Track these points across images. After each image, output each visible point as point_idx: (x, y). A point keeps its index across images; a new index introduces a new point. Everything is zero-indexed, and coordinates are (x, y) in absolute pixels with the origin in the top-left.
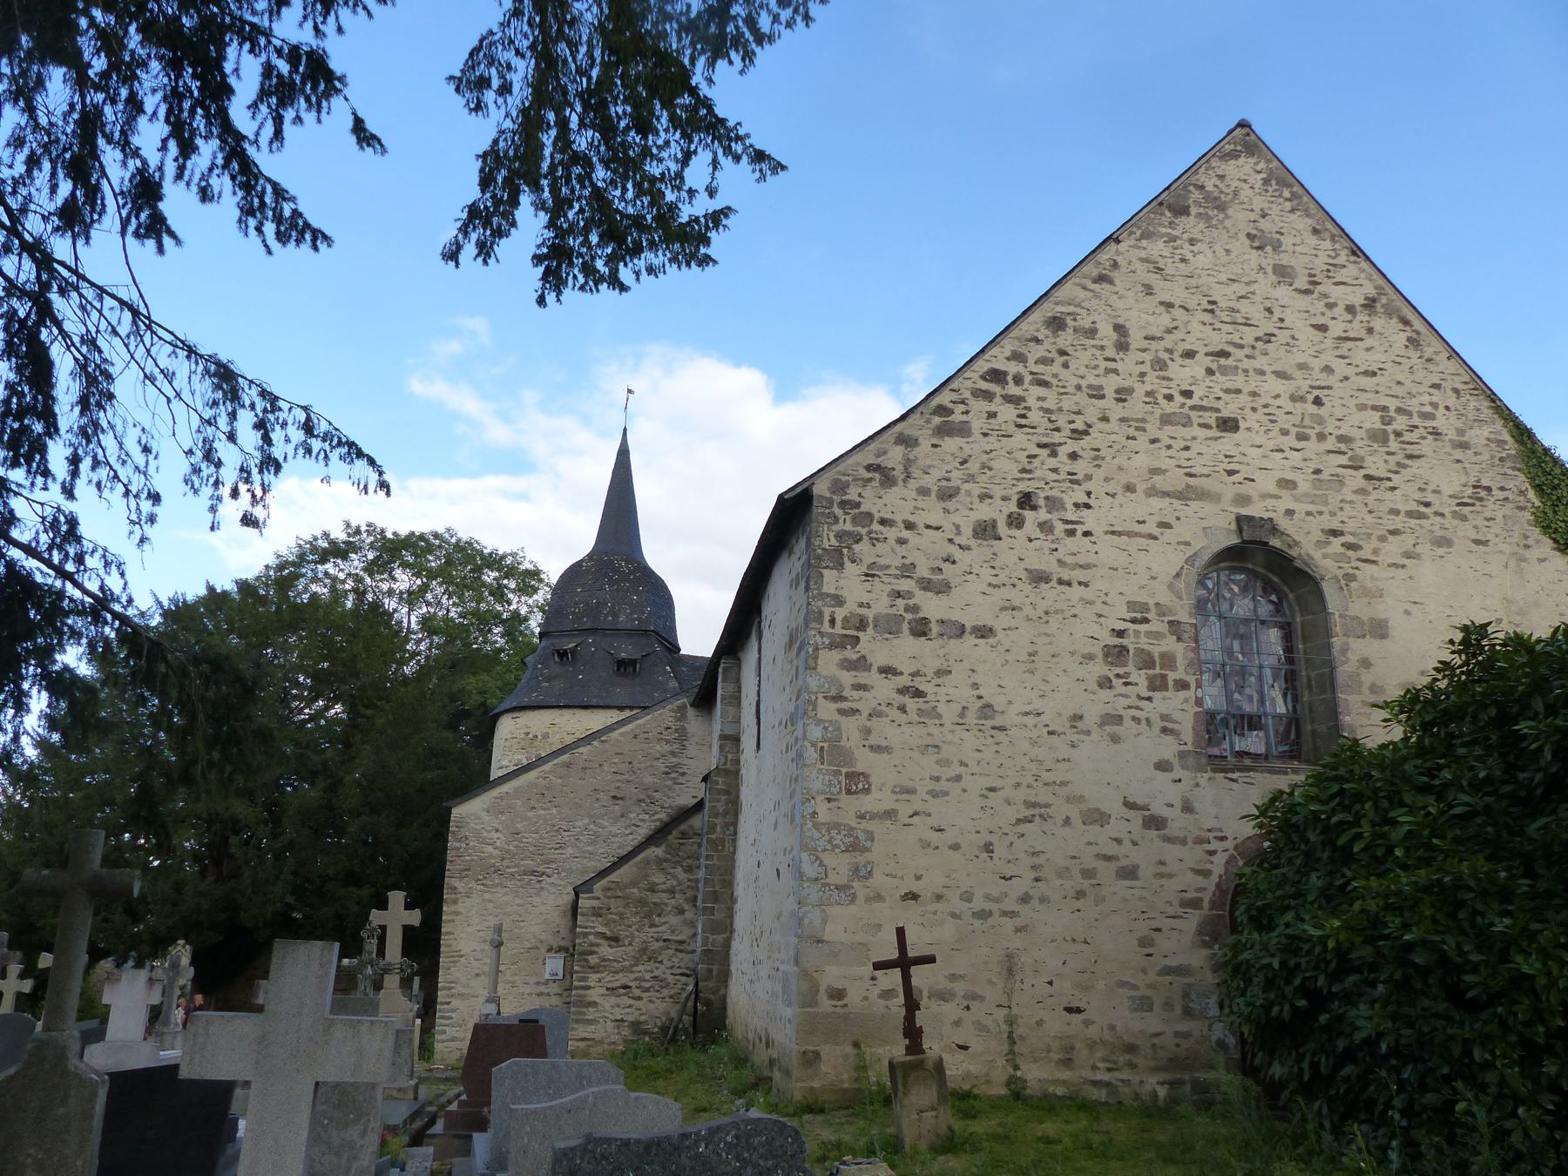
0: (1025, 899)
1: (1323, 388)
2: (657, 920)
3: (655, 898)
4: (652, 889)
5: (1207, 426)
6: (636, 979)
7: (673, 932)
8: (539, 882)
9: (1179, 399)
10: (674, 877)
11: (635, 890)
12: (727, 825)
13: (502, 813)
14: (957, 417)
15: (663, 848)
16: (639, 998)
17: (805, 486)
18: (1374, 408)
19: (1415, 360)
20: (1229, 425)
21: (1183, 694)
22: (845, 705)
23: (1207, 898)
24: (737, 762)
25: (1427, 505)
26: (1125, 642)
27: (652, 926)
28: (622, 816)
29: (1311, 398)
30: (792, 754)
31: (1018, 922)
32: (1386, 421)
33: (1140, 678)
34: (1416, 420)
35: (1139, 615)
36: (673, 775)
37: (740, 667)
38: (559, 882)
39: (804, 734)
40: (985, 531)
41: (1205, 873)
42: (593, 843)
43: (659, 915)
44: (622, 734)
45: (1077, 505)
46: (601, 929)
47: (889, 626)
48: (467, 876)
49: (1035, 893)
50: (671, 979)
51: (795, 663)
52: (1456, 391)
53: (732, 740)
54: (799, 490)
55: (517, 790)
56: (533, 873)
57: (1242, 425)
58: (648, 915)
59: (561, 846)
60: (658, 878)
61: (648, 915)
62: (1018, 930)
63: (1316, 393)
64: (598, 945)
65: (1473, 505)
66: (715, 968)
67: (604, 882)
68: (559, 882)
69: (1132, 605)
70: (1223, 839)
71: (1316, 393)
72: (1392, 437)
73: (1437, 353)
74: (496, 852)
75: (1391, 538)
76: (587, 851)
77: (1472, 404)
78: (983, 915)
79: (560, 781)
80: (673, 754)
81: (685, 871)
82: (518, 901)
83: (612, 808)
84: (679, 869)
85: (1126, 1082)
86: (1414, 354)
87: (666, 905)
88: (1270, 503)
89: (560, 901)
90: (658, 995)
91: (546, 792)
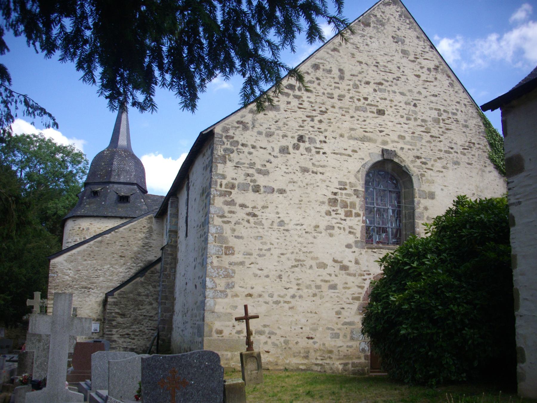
0: (293, 297)
2: (141, 307)
4: (139, 294)
6: (132, 331)
7: (148, 312)
8: (89, 291)
9: (363, 101)
10: (148, 290)
11: (132, 295)
12: (171, 268)
13: (72, 262)
15: (144, 278)
16: (134, 339)
17: (211, 129)
18: (436, 109)
19: (451, 92)
20: (381, 112)
21: (357, 219)
22: (225, 219)
24: (176, 242)
25: (452, 148)
26: (337, 197)
27: (139, 310)
28: (124, 264)
29: (412, 104)
31: (290, 305)
32: (440, 115)
34: (450, 115)
35: (343, 187)
36: (146, 247)
37: (178, 202)
40: (284, 150)
42: (111, 275)
43: (142, 305)
44: (125, 229)
45: (321, 141)
46: (117, 311)
47: (244, 188)
48: (57, 289)
50: (147, 331)
51: (205, 202)
52: (465, 105)
53: (174, 233)
54: (209, 130)
55: (79, 252)
56: (86, 288)
57: (386, 113)
58: (137, 305)
59: (98, 277)
60: (141, 290)
61: (137, 305)
63: (415, 102)
64: (116, 317)
66: (166, 327)
67: (118, 291)
69: (340, 183)
70: (369, 274)
72: (441, 121)
73: (459, 90)
74: (69, 279)
79: (97, 249)
82: (79, 299)
85: (328, 364)
87: (145, 301)
88: (395, 144)
90: (142, 338)
91: (91, 253)
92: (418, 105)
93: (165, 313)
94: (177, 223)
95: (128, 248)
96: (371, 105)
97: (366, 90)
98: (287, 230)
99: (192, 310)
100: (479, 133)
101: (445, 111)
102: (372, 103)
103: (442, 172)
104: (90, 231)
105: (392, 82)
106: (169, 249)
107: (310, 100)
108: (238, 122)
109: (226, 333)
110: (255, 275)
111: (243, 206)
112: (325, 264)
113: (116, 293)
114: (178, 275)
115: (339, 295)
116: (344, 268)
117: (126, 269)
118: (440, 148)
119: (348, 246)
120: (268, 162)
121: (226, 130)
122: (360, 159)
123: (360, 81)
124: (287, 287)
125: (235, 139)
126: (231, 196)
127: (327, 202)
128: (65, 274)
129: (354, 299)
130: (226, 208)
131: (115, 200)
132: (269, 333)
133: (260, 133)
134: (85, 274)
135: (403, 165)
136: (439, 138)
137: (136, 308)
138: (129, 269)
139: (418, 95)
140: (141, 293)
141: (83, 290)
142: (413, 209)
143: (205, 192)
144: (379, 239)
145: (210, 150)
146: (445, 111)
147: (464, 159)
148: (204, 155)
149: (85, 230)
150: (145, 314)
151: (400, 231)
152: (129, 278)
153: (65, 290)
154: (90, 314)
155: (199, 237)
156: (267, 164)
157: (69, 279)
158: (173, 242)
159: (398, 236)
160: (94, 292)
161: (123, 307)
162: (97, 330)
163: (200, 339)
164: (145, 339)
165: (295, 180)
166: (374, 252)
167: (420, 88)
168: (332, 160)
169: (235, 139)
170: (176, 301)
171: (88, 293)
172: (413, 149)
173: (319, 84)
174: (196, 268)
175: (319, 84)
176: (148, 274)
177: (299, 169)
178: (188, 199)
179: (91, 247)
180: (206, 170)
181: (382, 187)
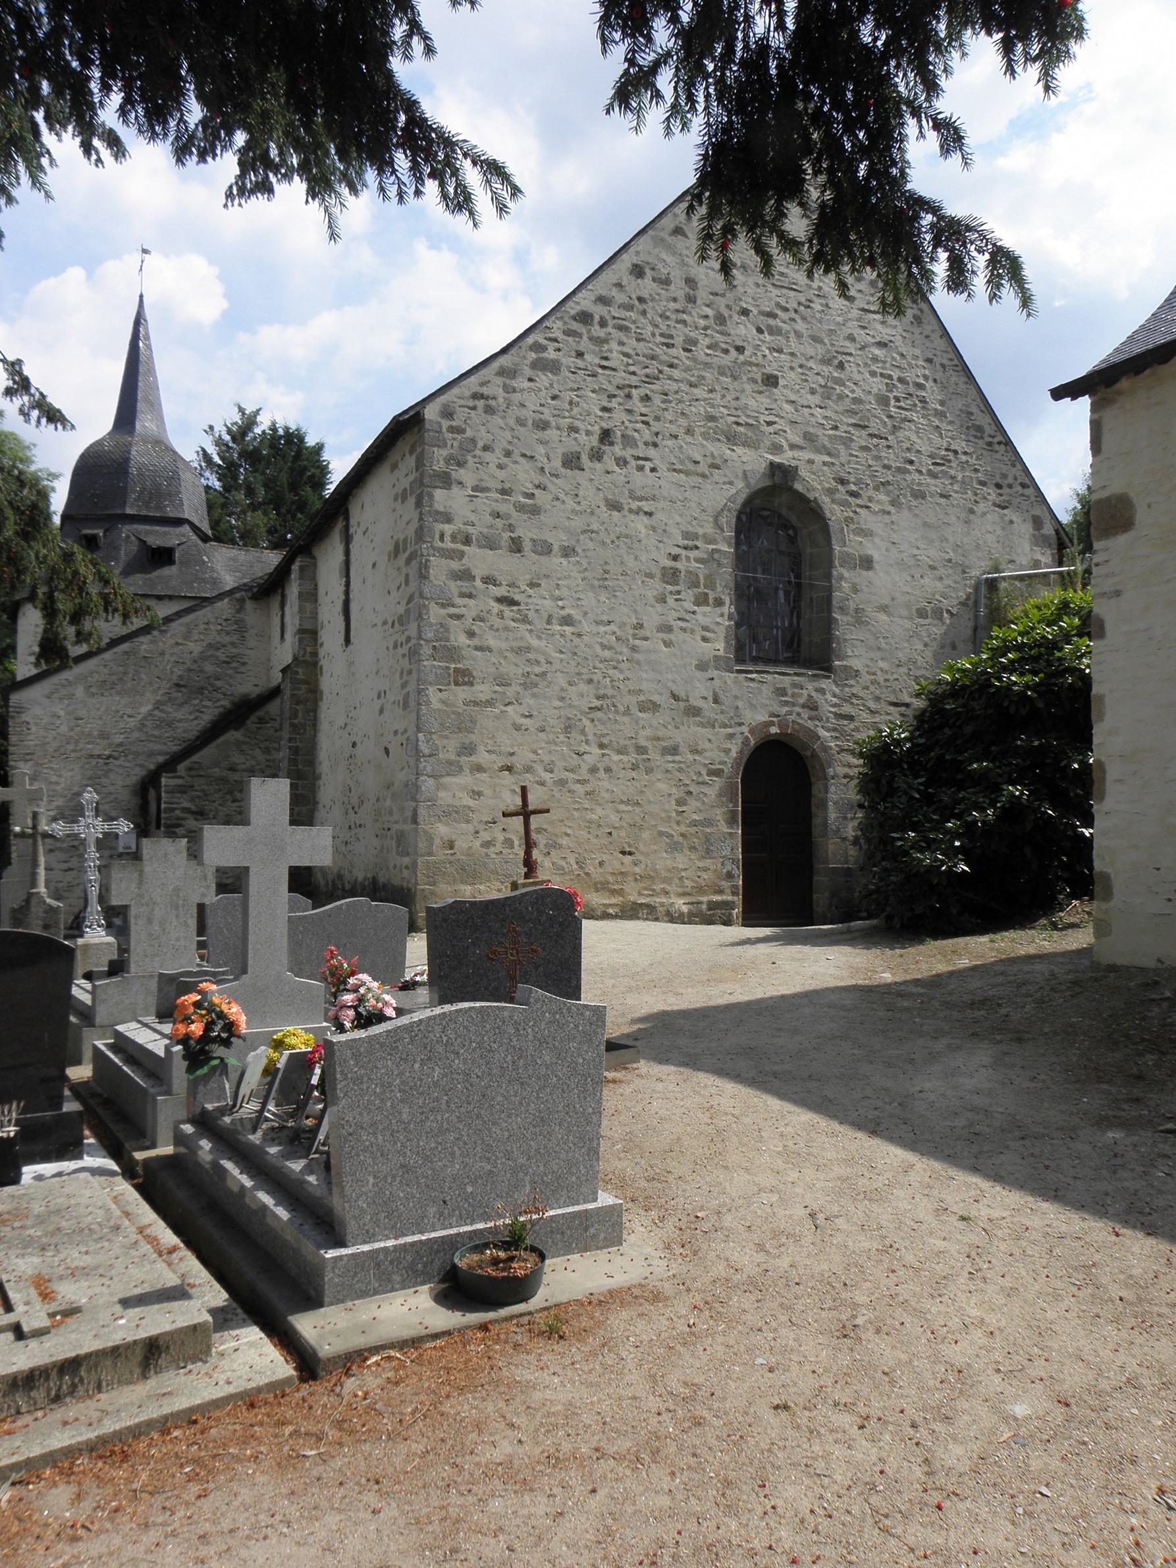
0: (593, 770)
1: (847, 354)
3: (235, 777)
4: (233, 769)
5: (754, 381)
9: (733, 353)
11: (217, 770)
14: (551, 354)
15: (242, 731)
17: (417, 409)
18: (882, 375)
19: (917, 335)
20: (771, 381)
21: (718, 610)
22: (452, 610)
23: (727, 769)
24: (315, 654)
25: (911, 462)
26: (678, 565)
27: (234, 801)
28: (186, 702)
29: (836, 362)
30: (404, 650)
31: (589, 788)
32: (890, 387)
33: (688, 595)
34: (912, 389)
35: (690, 543)
36: (234, 665)
37: (315, 566)
38: (127, 764)
39: (419, 631)
40: (572, 462)
41: (727, 751)
45: (646, 444)
46: (186, 805)
47: (490, 544)
49: (601, 766)
51: (404, 571)
52: (943, 366)
53: (310, 634)
54: (412, 413)
57: (781, 382)
60: (237, 758)
61: (231, 792)
62: (587, 793)
63: (840, 358)
65: (943, 465)
67: (186, 763)
68: (127, 764)
69: (686, 535)
70: (741, 724)
71: (840, 358)
72: (892, 402)
73: (933, 331)
75: (646, 296)
76: (152, 735)
77: (953, 379)
78: (562, 783)
80: (233, 644)
83: (175, 695)
84: (258, 751)
85: (662, 904)
86: (917, 331)
88: (797, 454)
89: (128, 782)
92: (846, 365)
94: (317, 614)
96: (751, 364)
97: (743, 330)
98: (579, 635)
99: (378, 800)
100: (968, 428)
101: (900, 380)
102: (753, 359)
103: (889, 513)
105: (796, 311)
106: (300, 671)
107: (626, 349)
108: (475, 396)
109: (461, 844)
110: (517, 728)
111: (489, 580)
112: (654, 703)
113: (181, 767)
114: (324, 726)
115: (682, 766)
116: (693, 711)
117: (190, 714)
118: (886, 462)
119: (702, 666)
120: (538, 487)
121: (448, 413)
122: (724, 483)
123: (729, 307)
124: (582, 750)
125: (469, 433)
126: (464, 561)
127: (659, 575)
129: (711, 773)
130: (454, 587)
131: (762, 470)
132: (546, 845)
133: (521, 422)
135: (811, 496)
136: (886, 439)
137: (228, 797)
139: (847, 343)
142: (829, 591)
143: (404, 551)
144: (758, 651)
145: (414, 457)
146: (900, 380)
147: (935, 486)
148: (394, 467)
151: (799, 636)
152: (197, 734)
153: (50, 762)
155: (391, 647)
156: (537, 492)
159: (795, 645)
160: (119, 766)
161: (199, 797)
163: (406, 860)
165: (595, 527)
166: (751, 679)
167: (853, 328)
168: (667, 482)
169: (469, 433)
170: (321, 782)
172: (833, 464)
173: (644, 313)
174: (386, 713)
175: (644, 313)
176: (251, 722)
177: (602, 504)
178: (347, 563)
180: (403, 502)
181: (765, 543)
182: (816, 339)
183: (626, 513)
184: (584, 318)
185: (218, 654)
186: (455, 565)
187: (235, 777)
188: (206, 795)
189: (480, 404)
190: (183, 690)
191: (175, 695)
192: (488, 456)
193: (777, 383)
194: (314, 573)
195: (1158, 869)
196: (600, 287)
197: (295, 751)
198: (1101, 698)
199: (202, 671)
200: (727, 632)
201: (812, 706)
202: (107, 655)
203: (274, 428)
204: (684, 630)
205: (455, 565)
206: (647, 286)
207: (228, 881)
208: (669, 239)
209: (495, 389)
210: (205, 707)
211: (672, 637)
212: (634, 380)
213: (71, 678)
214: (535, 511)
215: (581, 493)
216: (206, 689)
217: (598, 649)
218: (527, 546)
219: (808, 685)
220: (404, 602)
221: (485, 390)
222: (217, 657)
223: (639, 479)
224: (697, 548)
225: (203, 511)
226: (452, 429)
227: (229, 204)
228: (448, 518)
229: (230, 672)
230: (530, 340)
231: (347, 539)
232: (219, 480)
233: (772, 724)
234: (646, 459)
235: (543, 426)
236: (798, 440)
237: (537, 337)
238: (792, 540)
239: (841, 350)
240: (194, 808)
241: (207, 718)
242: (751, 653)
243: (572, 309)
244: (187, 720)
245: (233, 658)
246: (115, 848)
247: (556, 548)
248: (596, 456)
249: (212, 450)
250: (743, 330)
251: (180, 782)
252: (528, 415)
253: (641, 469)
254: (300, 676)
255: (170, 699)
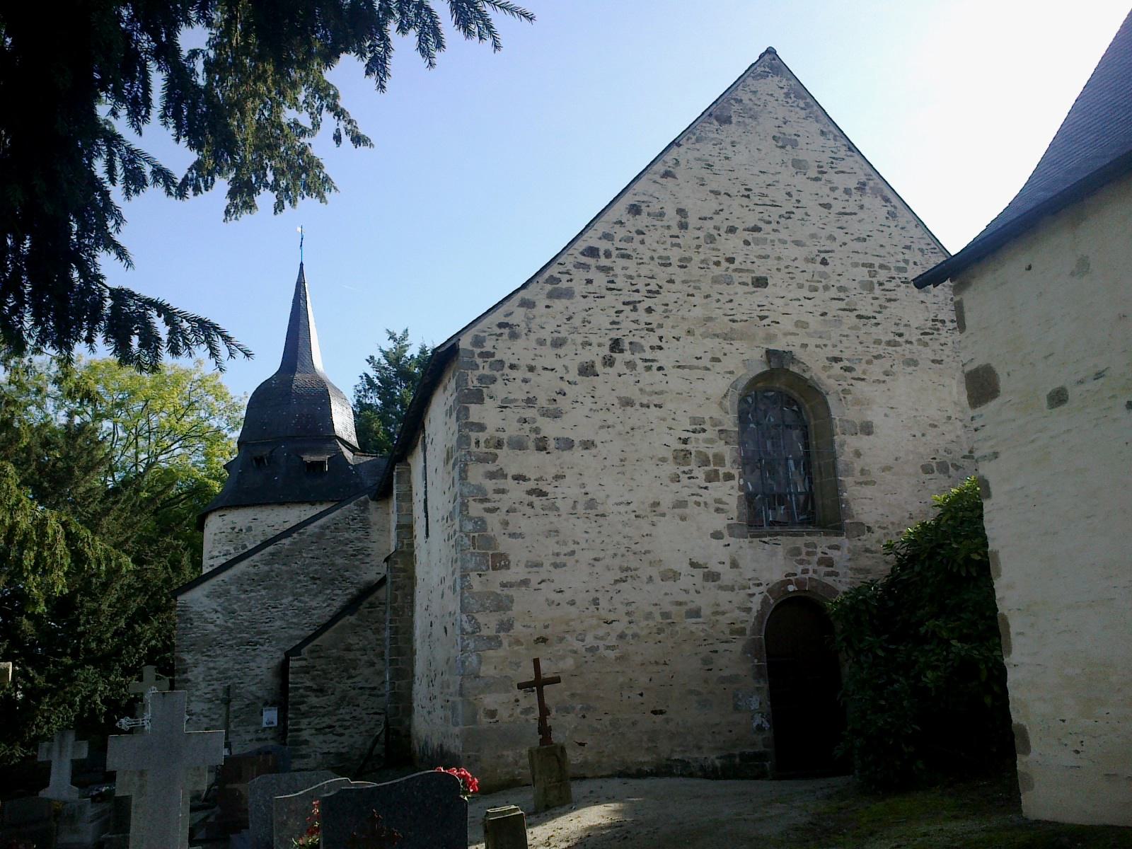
1: (828, 252)
3: (351, 655)
4: (348, 649)
9: (724, 264)
14: (564, 284)
17: (453, 342)
18: (864, 265)
19: (893, 228)
20: (761, 282)
22: (487, 505)
25: (901, 335)
29: (819, 259)
34: (894, 273)
35: (698, 427)
36: (360, 557)
37: (410, 472)
38: (271, 649)
40: (587, 370)
41: (749, 610)
43: (355, 669)
45: (652, 348)
46: (308, 684)
47: (519, 445)
48: (193, 650)
50: (365, 717)
52: (921, 250)
53: (406, 529)
54: (448, 345)
61: (346, 670)
63: (823, 255)
65: (933, 334)
68: (271, 649)
69: (694, 420)
72: (876, 286)
74: (216, 629)
81: (374, 634)
83: (311, 586)
85: (696, 760)
86: (892, 224)
88: (791, 339)
90: (356, 730)
93: (398, 680)
95: (325, 561)
96: (741, 271)
102: (742, 267)
104: (253, 532)
106: (399, 560)
107: (628, 272)
108: (501, 325)
113: (305, 650)
116: (712, 577)
117: (324, 602)
119: (717, 535)
121: (478, 342)
126: (497, 463)
128: (206, 621)
132: (582, 709)
133: (541, 342)
134: (244, 617)
138: (329, 601)
140: (352, 645)
141: (244, 648)
149: (244, 531)
150: (360, 685)
154: (259, 694)
157: (216, 629)
158: (405, 546)
159: (810, 508)
162: (272, 723)
164: (365, 734)
169: (497, 357)
171: (253, 653)
173: (642, 242)
175: (642, 242)
179: (255, 566)
182: (798, 243)
183: (639, 407)
184: (592, 252)
185: (347, 548)
186: (491, 467)
187: (351, 655)
188: (325, 674)
189: (506, 331)
190: (318, 582)
191: (311, 586)
192: (513, 374)
193: (767, 284)
194: (409, 477)
195: (1064, 721)
196: (601, 227)
197: (395, 631)
198: (996, 553)
199: (333, 564)
200: (739, 502)
201: (828, 562)
202: (256, 557)
203: (423, 351)
204: (698, 504)
205: (491, 467)
206: (642, 221)
207: (343, 750)
208: (661, 180)
209: (518, 317)
210: (337, 595)
211: (687, 511)
212: (636, 297)
213: (226, 579)
214: (556, 415)
215: (597, 394)
216: (337, 580)
217: (620, 526)
218: (552, 444)
219: (823, 543)
220: (452, 502)
221: (510, 320)
222: (346, 551)
223: (646, 378)
224: (704, 431)
225: (351, 429)
226: (482, 355)
227: (228, 218)
228: (481, 427)
229: (357, 563)
230: (546, 275)
231: (425, 450)
232: (379, 398)
233: (790, 582)
234: (653, 361)
235: (558, 343)
236: (792, 329)
237: (554, 271)
238: (798, 413)
239: (823, 249)
240: (315, 687)
241: (337, 604)
242: (767, 518)
243: (581, 245)
244: (320, 608)
245: (359, 551)
246: (260, 724)
247: (577, 443)
248: (609, 362)
249: (373, 373)
250: (731, 245)
251: (303, 663)
252: (546, 335)
253: (649, 369)
254: (400, 566)
255: (307, 591)
